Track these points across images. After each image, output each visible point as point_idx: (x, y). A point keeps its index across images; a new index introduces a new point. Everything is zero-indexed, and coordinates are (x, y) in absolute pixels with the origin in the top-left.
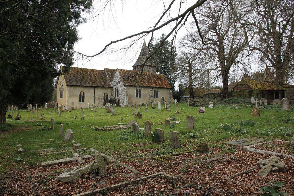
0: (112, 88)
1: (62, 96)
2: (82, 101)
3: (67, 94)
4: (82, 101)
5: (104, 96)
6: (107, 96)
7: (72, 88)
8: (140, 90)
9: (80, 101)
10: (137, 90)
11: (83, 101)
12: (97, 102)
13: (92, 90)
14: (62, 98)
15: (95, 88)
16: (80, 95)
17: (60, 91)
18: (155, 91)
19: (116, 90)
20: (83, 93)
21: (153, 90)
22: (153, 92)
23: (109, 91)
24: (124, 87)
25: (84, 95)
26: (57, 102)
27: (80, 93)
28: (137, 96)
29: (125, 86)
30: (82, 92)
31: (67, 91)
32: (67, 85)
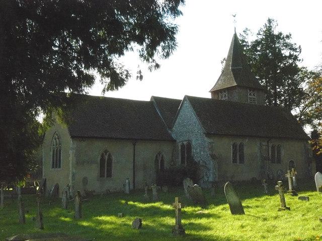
0: (173, 141)
1: (57, 163)
2: (238, 161)
3: (71, 158)
4: (238, 161)
5: (156, 160)
6: (162, 161)
7: (84, 144)
8: (241, 146)
9: (102, 175)
10: (234, 146)
11: (109, 175)
12: (140, 177)
13: (128, 149)
14: (56, 169)
15: (134, 141)
16: (102, 160)
17: (51, 153)
18: (273, 147)
19: (183, 146)
20: (110, 155)
21: (270, 145)
22: (270, 148)
23: (166, 150)
24: (206, 139)
25: (110, 160)
26: (44, 178)
27: (102, 156)
28: (235, 161)
29: (208, 135)
30: (106, 152)
31: (71, 152)
32: (73, 137)
